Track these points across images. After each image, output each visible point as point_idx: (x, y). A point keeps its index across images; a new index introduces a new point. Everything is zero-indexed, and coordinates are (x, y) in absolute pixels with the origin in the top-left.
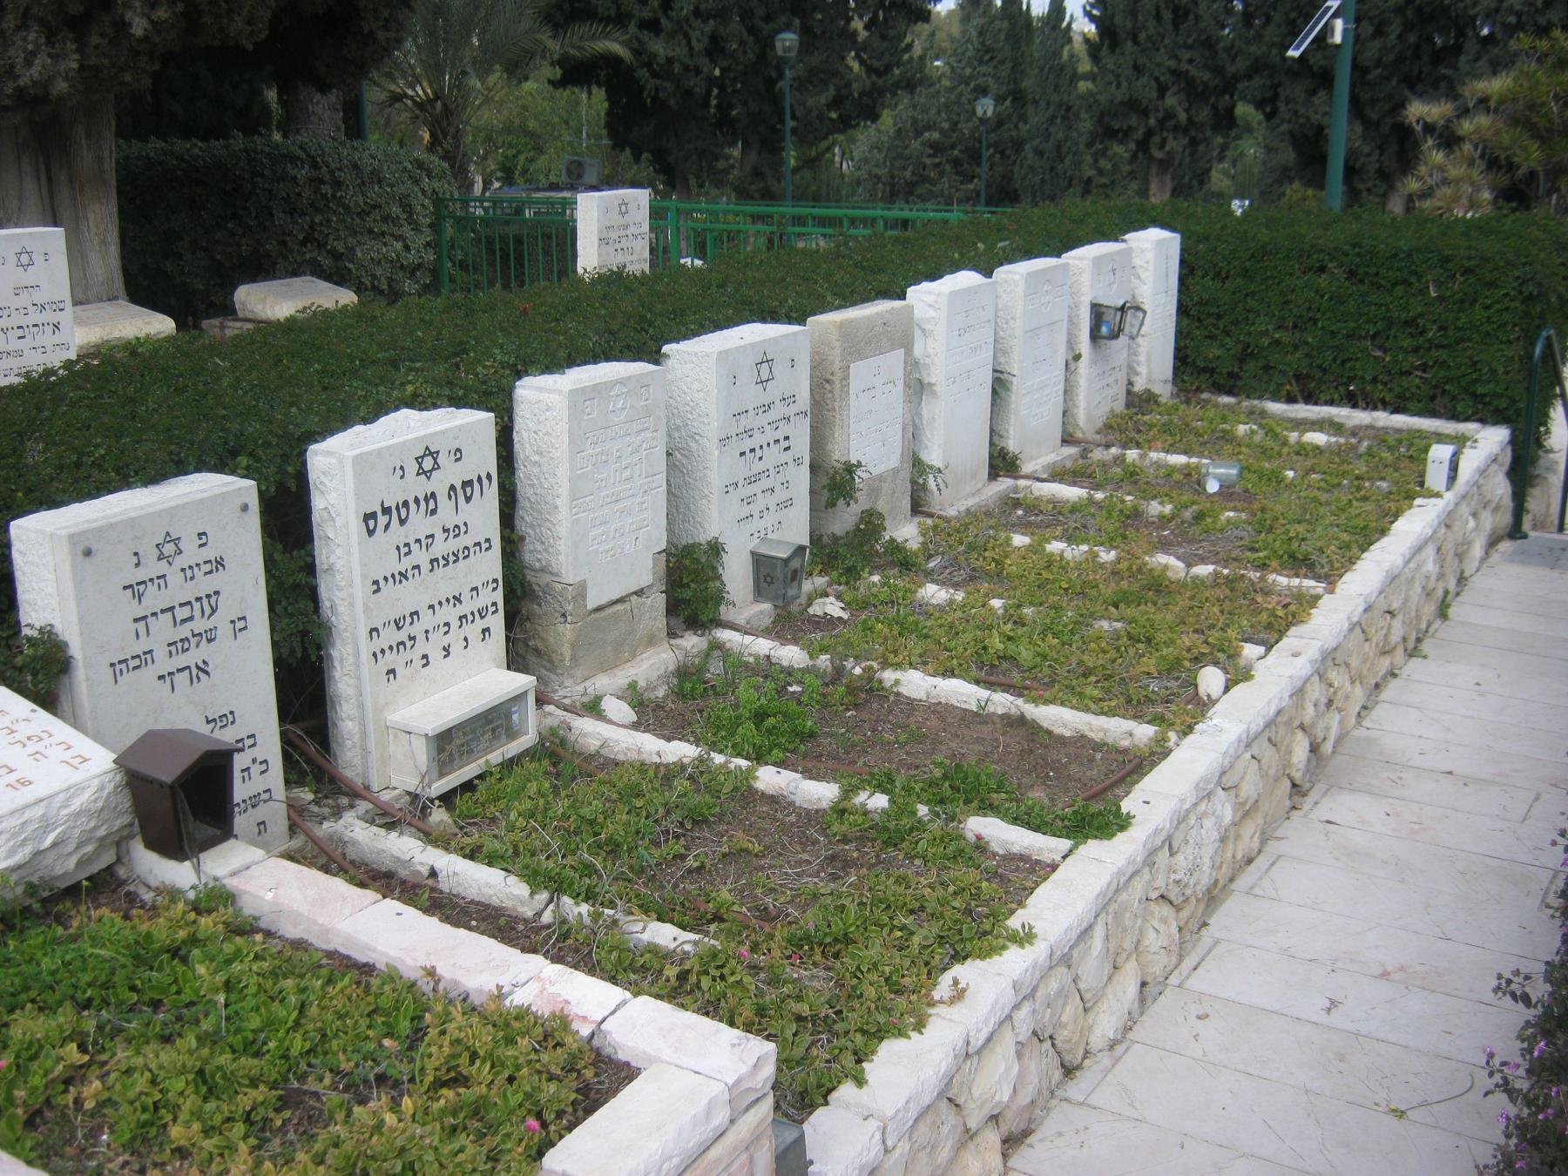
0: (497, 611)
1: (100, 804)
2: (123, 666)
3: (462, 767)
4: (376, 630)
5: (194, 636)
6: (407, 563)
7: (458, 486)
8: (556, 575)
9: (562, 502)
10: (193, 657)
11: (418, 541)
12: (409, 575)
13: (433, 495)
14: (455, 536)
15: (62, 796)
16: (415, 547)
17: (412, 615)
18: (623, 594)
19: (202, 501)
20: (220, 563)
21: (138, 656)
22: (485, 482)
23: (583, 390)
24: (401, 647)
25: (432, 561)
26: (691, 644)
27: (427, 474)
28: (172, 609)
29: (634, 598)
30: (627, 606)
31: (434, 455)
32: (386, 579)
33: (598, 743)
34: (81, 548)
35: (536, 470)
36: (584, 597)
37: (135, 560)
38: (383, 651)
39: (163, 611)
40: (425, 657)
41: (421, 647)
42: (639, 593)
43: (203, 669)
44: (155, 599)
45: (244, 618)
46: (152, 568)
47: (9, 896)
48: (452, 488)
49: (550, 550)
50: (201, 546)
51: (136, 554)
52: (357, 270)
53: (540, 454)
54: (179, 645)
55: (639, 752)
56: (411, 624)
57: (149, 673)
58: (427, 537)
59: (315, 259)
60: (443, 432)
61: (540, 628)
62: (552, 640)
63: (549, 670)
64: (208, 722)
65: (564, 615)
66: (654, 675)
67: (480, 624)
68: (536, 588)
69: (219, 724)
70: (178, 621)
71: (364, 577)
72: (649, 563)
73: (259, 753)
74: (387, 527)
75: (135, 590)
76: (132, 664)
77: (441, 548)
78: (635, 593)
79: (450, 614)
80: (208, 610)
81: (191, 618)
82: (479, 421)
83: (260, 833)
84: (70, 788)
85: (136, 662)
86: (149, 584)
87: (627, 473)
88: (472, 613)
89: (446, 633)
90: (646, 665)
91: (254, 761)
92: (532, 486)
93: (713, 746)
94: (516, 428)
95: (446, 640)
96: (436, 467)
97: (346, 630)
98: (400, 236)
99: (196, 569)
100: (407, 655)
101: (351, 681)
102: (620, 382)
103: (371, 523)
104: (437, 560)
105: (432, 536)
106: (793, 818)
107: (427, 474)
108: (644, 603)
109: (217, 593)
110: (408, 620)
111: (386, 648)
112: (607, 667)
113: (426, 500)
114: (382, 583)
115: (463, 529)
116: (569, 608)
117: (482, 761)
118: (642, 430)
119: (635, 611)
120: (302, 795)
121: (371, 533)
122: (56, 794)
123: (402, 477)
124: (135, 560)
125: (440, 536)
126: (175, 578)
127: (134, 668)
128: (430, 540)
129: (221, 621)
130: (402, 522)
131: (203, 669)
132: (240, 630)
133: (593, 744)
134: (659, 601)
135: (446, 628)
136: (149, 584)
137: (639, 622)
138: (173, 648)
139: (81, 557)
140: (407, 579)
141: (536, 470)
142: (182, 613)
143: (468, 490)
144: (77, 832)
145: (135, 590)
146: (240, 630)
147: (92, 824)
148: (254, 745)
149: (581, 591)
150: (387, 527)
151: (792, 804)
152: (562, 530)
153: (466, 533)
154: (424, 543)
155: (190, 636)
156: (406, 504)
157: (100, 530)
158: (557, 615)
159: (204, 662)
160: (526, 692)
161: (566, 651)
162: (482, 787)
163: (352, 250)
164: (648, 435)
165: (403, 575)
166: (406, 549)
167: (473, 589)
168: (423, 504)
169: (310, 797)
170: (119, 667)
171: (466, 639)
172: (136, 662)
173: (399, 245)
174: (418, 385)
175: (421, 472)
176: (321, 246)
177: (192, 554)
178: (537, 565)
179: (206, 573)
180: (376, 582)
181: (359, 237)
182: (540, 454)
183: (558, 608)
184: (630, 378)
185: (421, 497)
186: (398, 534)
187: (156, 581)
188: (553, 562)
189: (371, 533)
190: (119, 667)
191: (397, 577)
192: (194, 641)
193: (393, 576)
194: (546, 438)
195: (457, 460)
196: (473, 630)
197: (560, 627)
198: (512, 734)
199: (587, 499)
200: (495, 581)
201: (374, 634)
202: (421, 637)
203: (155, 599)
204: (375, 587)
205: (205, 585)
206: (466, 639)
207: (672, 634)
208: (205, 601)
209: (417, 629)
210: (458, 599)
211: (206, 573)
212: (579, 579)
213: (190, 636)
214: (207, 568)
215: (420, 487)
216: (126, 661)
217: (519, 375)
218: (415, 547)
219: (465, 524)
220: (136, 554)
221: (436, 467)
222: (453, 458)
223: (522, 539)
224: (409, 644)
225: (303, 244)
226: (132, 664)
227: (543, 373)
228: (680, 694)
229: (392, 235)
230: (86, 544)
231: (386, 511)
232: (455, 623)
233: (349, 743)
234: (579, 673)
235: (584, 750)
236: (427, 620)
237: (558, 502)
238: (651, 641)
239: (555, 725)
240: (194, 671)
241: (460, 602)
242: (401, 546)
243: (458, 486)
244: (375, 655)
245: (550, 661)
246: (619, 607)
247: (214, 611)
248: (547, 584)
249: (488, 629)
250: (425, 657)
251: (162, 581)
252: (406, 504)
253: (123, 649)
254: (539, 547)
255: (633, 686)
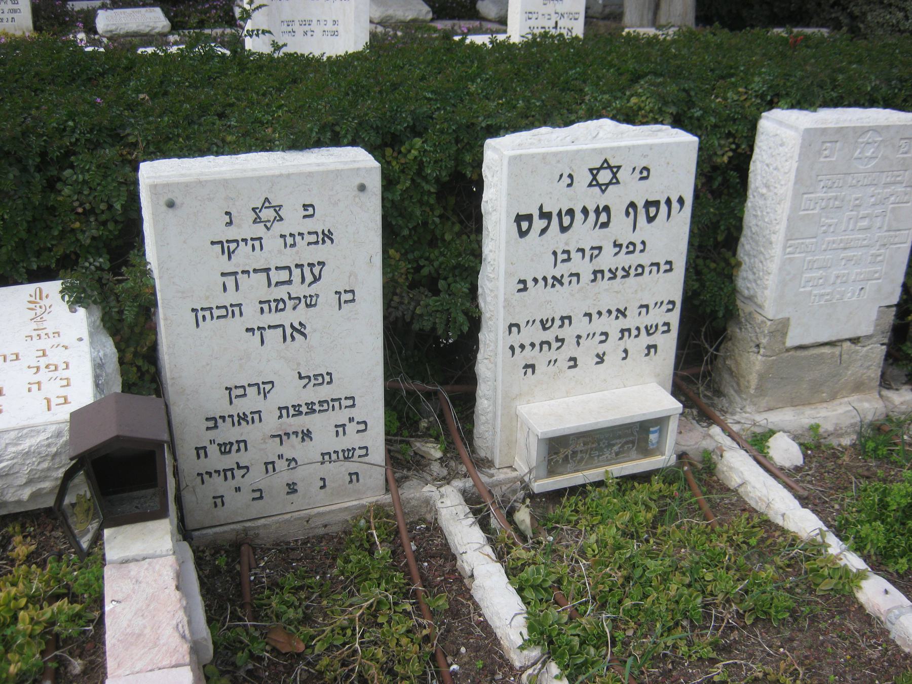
0: (668, 331)
1: (54, 450)
2: (207, 314)
3: (576, 471)
4: (518, 326)
5: (290, 298)
6: (563, 269)
7: (640, 204)
8: (760, 307)
9: (778, 239)
10: (289, 317)
11: (582, 251)
12: (566, 280)
13: (607, 209)
14: (628, 253)
15: (13, 435)
16: (576, 256)
17: (562, 319)
18: (834, 339)
19: (310, 175)
20: (328, 236)
21: (225, 307)
22: (675, 205)
23: (824, 131)
24: (545, 347)
25: (595, 273)
26: (902, 399)
27: (604, 187)
28: (267, 270)
29: (847, 345)
30: (837, 350)
31: (615, 170)
32: (535, 280)
33: (739, 481)
34: (163, 200)
35: (761, 202)
36: (784, 334)
37: (227, 219)
38: (522, 347)
39: (255, 271)
40: (574, 359)
41: (569, 350)
42: (855, 341)
43: (300, 330)
44: (244, 257)
45: (352, 292)
46: (246, 229)
47: (10, 497)
48: (632, 205)
49: (759, 282)
50: (305, 217)
51: (227, 213)
52: (866, 29)
53: (767, 186)
54: (273, 305)
55: (768, 506)
56: (561, 326)
57: (236, 325)
58: (593, 248)
59: (837, 18)
60: (629, 148)
61: (736, 351)
62: (743, 366)
63: (736, 391)
64: (301, 377)
65: (758, 346)
66: (846, 422)
67: (645, 340)
68: (742, 314)
69: (313, 381)
70: (273, 282)
71: (509, 274)
72: (874, 315)
73: (358, 414)
74: (544, 231)
75: (227, 248)
76: (216, 313)
77: (607, 260)
78: (851, 340)
79: (614, 326)
80: (309, 278)
81: (290, 282)
82: (678, 144)
83: (351, 481)
84: (23, 428)
85: (223, 312)
86: (242, 244)
87: (865, 223)
88: (638, 329)
89: (601, 342)
90: (841, 410)
91: (351, 420)
92: (756, 216)
93: (840, 533)
94: (754, 157)
95: (601, 349)
96: (615, 181)
97: (490, 318)
98: (904, 9)
99: (298, 238)
100: (547, 354)
101: (490, 366)
102: (876, 130)
103: (525, 225)
104: (602, 272)
105: (600, 248)
106: (875, 654)
107: (604, 187)
108: (857, 352)
109: (321, 264)
110: (558, 323)
111: (604, 312)
112: (795, 402)
113: (597, 211)
114: (530, 284)
115: (639, 247)
116: (764, 341)
117: (603, 470)
118: (894, 183)
119: (845, 357)
120: (432, 451)
121: (523, 234)
122: (7, 431)
123: (569, 185)
124: (227, 219)
125: (608, 249)
126: (272, 242)
127: (218, 317)
128: (596, 252)
129: (325, 289)
130: (564, 229)
131: (300, 330)
132: (346, 302)
133: (734, 481)
134: (877, 351)
135: (603, 338)
136: (242, 244)
137: (847, 368)
138: (266, 307)
139: (165, 208)
140: (562, 284)
141: (761, 202)
142: (276, 276)
143: (652, 211)
144: (26, 470)
145: (227, 248)
146: (346, 302)
147: (45, 465)
148: (353, 406)
149: (782, 328)
150: (544, 231)
151: (885, 632)
152: (773, 266)
153: (642, 251)
154: (588, 254)
155: (286, 298)
156: (571, 212)
157: (187, 185)
158: (752, 344)
159: (300, 324)
160: (668, 417)
161: (753, 380)
162: (594, 494)
163: (864, 14)
164: (900, 189)
165: (558, 280)
166: (565, 256)
167: (642, 306)
168: (592, 216)
169: (438, 454)
170: (200, 314)
171: (626, 351)
172: (223, 312)
173: (901, 15)
174: (644, 98)
175: (594, 182)
176: (844, 9)
177: (293, 221)
178: (746, 293)
179: (309, 244)
180: (524, 282)
181: (872, 5)
182: (767, 186)
183: (754, 339)
184: (888, 127)
185: (591, 208)
186: (555, 239)
187: (250, 243)
188: (759, 294)
189: (523, 234)
190: (200, 314)
191: (550, 281)
192: (290, 304)
193: (545, 279)
194: (775, 172)
195: (642, 179)
196: (638, 345)
197: (753, 357)
198: (646, 452)
199: (808, 241)
200: (672, 303)
201: (514, 329)
202: (571, 341)
203: (244, 257)
204: (521, 286)
205: (307, 254)
206: (626, 351)
207: (886, 382)
208: (307, 270)
209: (568, 333)
210: (622, 313)
211: (309, 244)
212: (780, 316)
213: (286, 298)
214: (313, 238)
215: (593, 199)
216: (210, 309)
217: (771, 105)
218: (576, 256)
219: (643, 243)
220: (227, 213)
221: (615, 181)
222: (637, 175)
223: (739, 264)
224: (555, 345)
225: (832, 6)
226: (216, 313)
227: (792, 107)
228: (859, 448)
229: (897, 7)
230: (170, 196)
231: (545, 215)
232: (614, 334)
233: (483, 419)
234: (763, 402)
235: (727, 483)
236: (580, 326)
237: (774, 238)
238: (858, 387)
239: (711, 448)
240: (289, 331)
241: (625, 316)
242: (559, 252)
243: (640, 204)
244: (512, 348)
245: (738, 384)
246: (826, 350)
247: (316, 279)
248: (750, 313)
249: (655, 347)
250: (574, 359)
251: (257, 244)
252: (571, 212)
253: (208, 298)
254: (751, 277)
255: (814, 428)
